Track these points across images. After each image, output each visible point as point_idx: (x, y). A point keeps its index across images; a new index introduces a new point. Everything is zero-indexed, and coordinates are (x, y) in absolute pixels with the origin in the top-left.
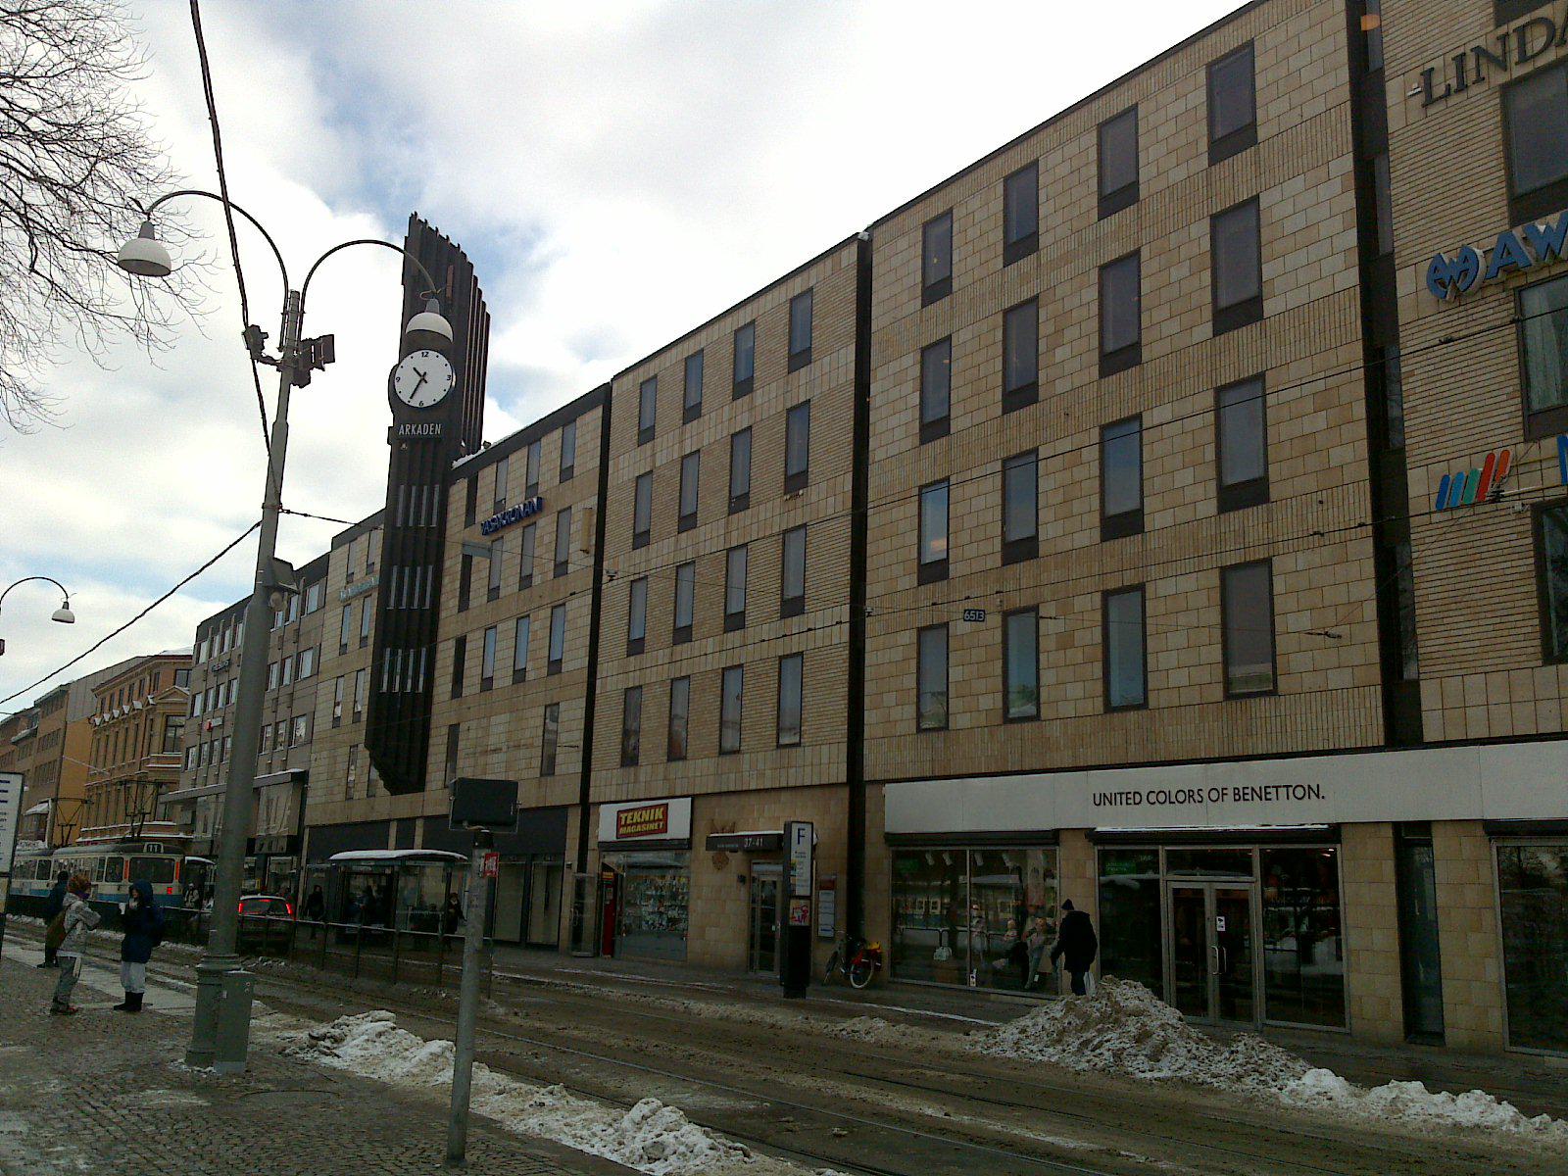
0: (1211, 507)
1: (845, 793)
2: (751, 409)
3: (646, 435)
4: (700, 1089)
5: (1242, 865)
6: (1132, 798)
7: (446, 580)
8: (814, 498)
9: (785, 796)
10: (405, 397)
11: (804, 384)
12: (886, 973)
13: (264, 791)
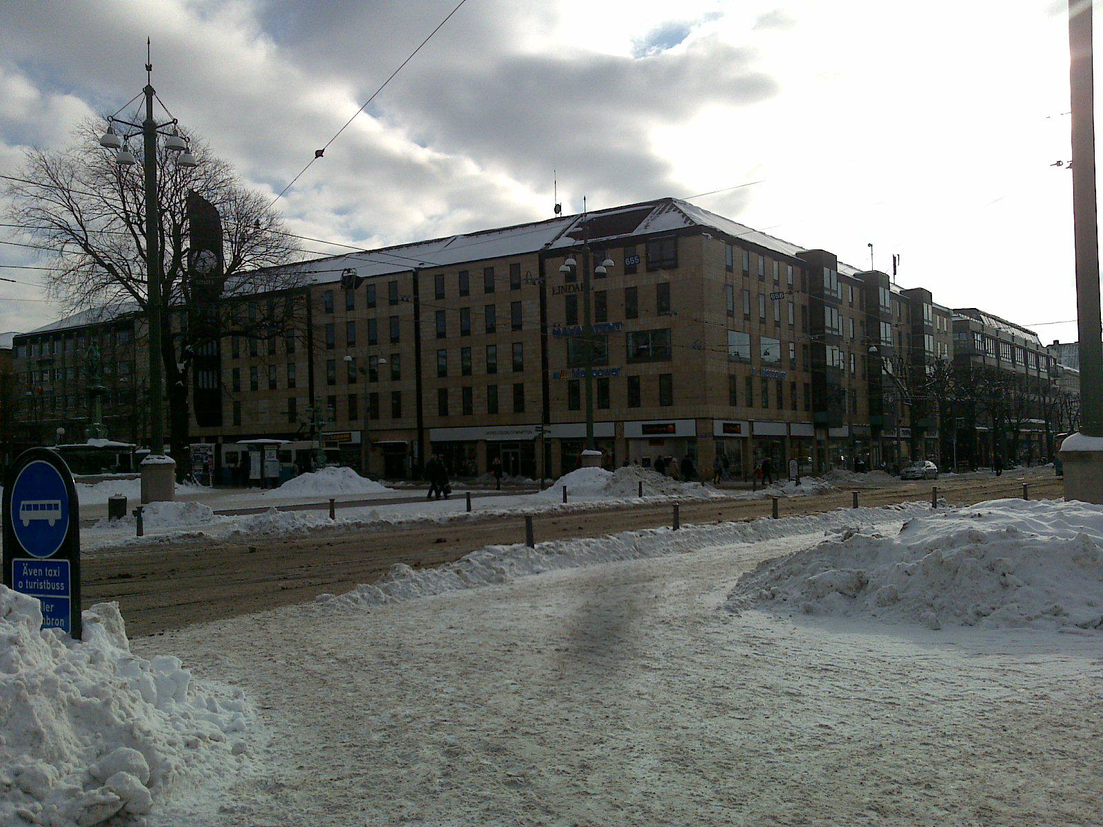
4: (1024, 409)
5: (517, 447)
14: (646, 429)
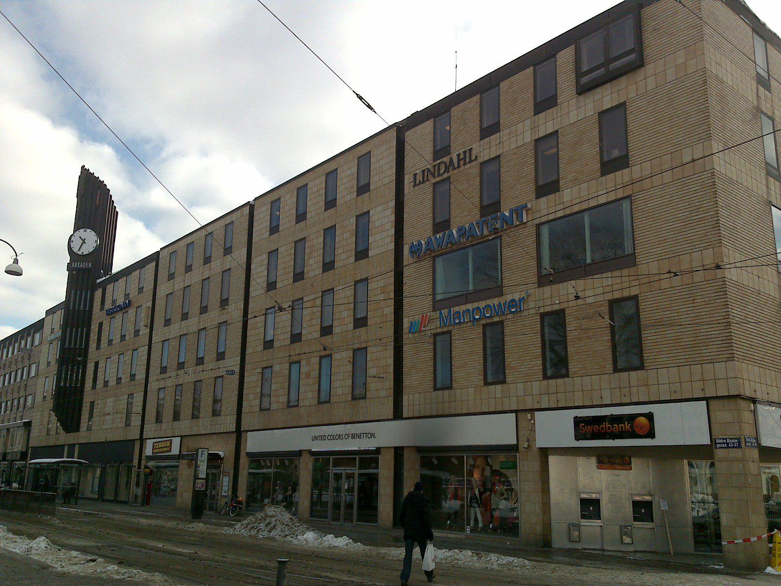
0: (351, 326)
1: (234, 436)
2: (210, 269)
3: (171, 276)
6: (322, 438)
7: (92, 335)
8: (230, 311)
9: (214, 436)
10: (75, 250)
11: (229, 262)
12: (244, 509)
13: (11, 430)
14: (586, 427)
